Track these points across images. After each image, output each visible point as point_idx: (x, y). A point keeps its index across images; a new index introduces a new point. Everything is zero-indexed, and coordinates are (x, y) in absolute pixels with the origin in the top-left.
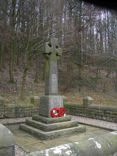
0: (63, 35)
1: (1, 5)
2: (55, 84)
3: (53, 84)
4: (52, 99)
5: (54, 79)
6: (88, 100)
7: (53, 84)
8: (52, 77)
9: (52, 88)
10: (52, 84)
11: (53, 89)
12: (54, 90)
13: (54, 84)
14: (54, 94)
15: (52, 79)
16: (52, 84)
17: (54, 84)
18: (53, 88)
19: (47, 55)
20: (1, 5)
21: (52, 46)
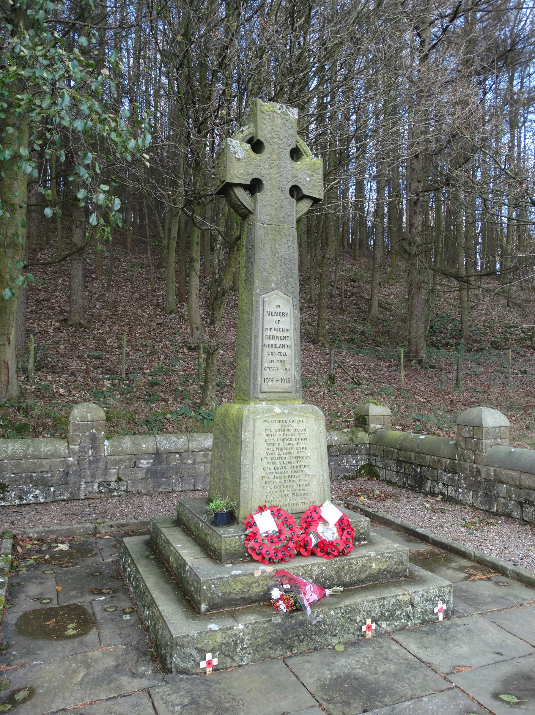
0: (215, 156)
1: (3, 67)
2: (284, 342)
3: (272, 342)
4: (259, 423)
5: (277, 318)
6: (480, 427)
7: (272, 342)
8: (267, 309)
9: (266, 365)
10: (266, 342)
11: (270, 369)
12: (281, 374)
13: (279, 342)
14: (272, 396)
15: (267, 318)
16: (266, 342)
17: (279, 342)
18: (272, 365)
19: (242, 195)
20: (3, 67)
21: (268, 148)
